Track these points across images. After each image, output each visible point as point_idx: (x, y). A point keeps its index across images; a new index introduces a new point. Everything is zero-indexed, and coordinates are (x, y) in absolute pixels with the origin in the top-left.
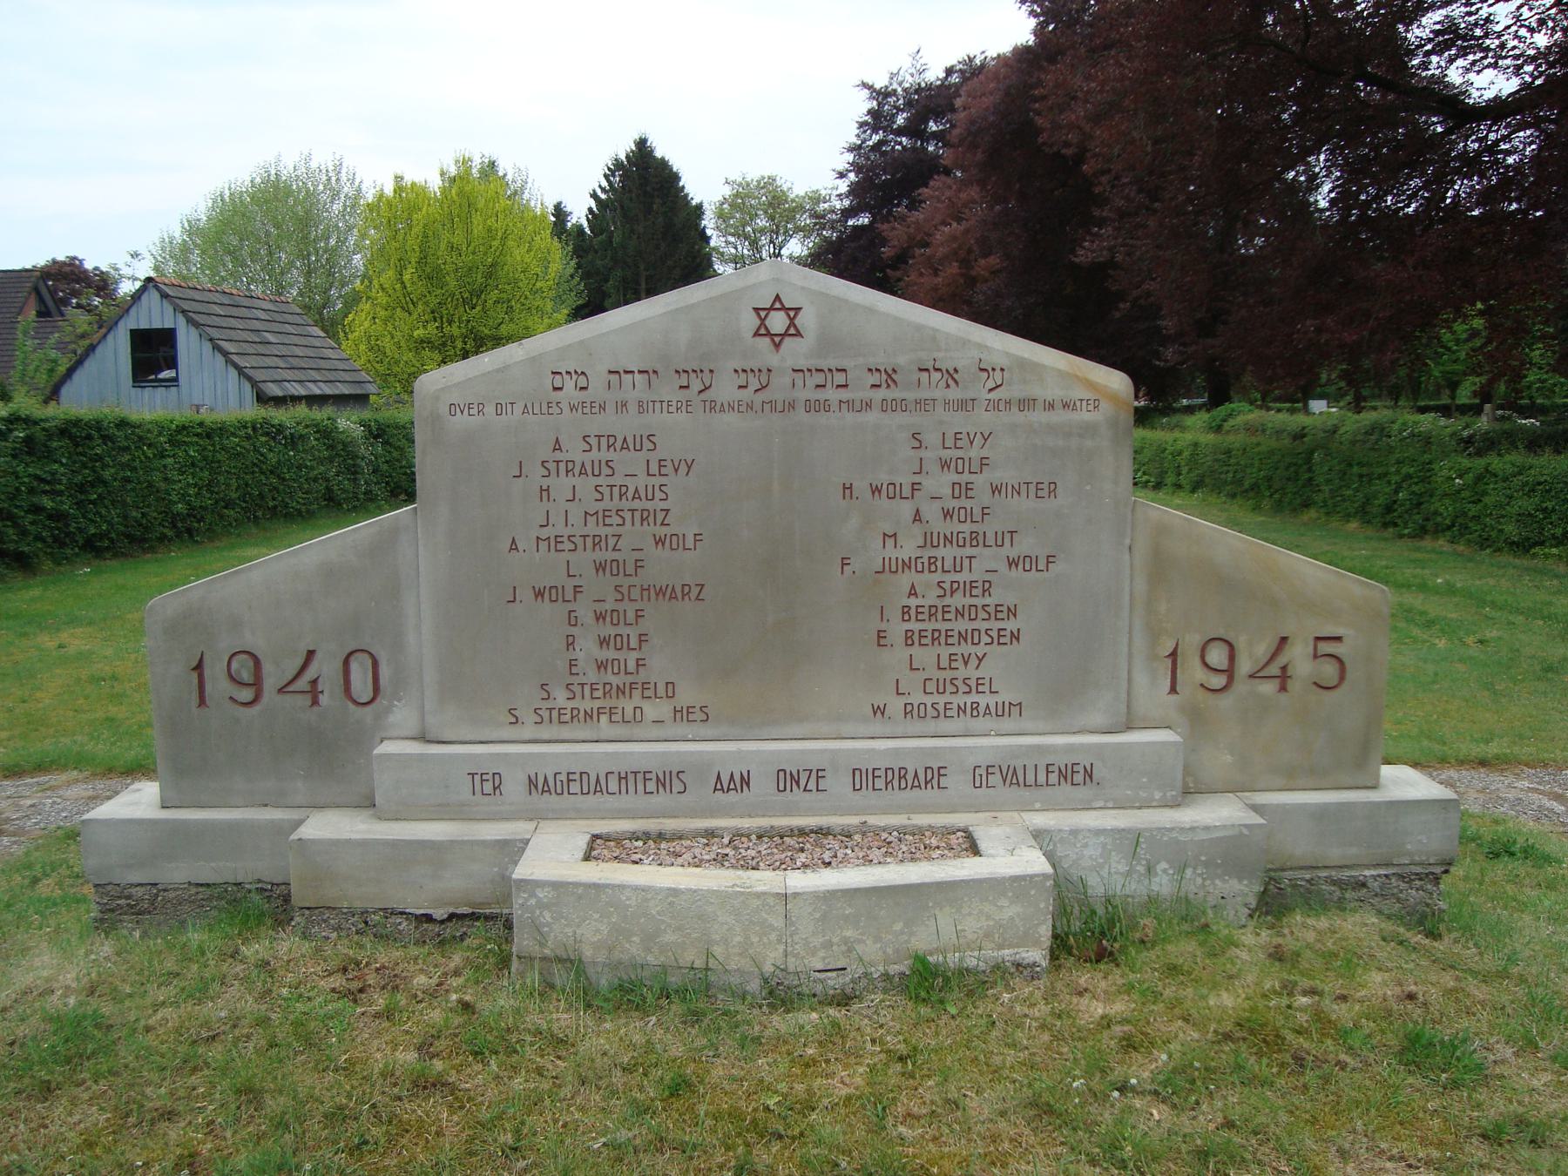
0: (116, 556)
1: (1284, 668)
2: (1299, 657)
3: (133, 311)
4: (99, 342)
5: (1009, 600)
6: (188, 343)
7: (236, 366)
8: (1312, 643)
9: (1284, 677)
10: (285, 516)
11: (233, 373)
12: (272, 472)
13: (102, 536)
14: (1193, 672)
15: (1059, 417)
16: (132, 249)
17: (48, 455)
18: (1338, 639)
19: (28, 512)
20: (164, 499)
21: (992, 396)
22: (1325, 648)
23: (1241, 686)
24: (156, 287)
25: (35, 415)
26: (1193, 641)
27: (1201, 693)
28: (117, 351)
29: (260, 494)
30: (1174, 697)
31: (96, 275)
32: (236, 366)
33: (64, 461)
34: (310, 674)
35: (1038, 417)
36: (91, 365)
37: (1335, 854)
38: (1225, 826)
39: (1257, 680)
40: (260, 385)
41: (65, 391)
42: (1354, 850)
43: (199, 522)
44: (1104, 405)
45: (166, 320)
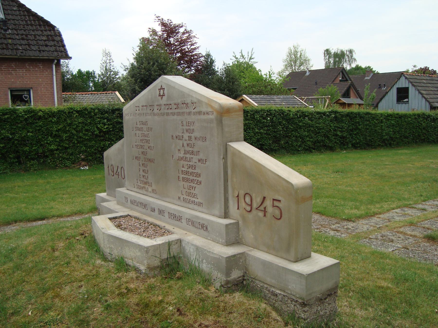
0: (361, 149)
1: (265, 208)
2: (268, 203)
3: (398, 83)
4: (388, 91)
5: (199, 172)
6: (412, 91)
7: (424, 98)
8: (272, 201)
9: (265, 211)
10: (428, 142)
11: (424, 100)
12: (424, 129)
13: (357, 144)
14: (243, 204)
15: (206, 117)
16: (414, 64)
17: (342, 121)
18: (280, 201)
19: (334, 136)
20: (381, 135)
21: (194, 111)
22: (276, 203)
23: (254, 212)
24: (404, 76)
25: (338, 111)
26: (242, 193)
27: (244, 211)
28: (393, 94)
29: (418, 135)
30: (238, 211)
31: (432, 72)
32: (424, 98)
33: (347, 123)
34: (118, 172)
35: (202, 117)
36: (386, 98)
37: (269, 280)
38: (216, 254)
39: (258, 211)
40: (431, 103)
41: (380, 105)
42: (273, 281)
43: (394, 141)
44: (215, 113)
45: (406, 85)
